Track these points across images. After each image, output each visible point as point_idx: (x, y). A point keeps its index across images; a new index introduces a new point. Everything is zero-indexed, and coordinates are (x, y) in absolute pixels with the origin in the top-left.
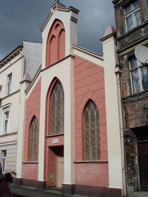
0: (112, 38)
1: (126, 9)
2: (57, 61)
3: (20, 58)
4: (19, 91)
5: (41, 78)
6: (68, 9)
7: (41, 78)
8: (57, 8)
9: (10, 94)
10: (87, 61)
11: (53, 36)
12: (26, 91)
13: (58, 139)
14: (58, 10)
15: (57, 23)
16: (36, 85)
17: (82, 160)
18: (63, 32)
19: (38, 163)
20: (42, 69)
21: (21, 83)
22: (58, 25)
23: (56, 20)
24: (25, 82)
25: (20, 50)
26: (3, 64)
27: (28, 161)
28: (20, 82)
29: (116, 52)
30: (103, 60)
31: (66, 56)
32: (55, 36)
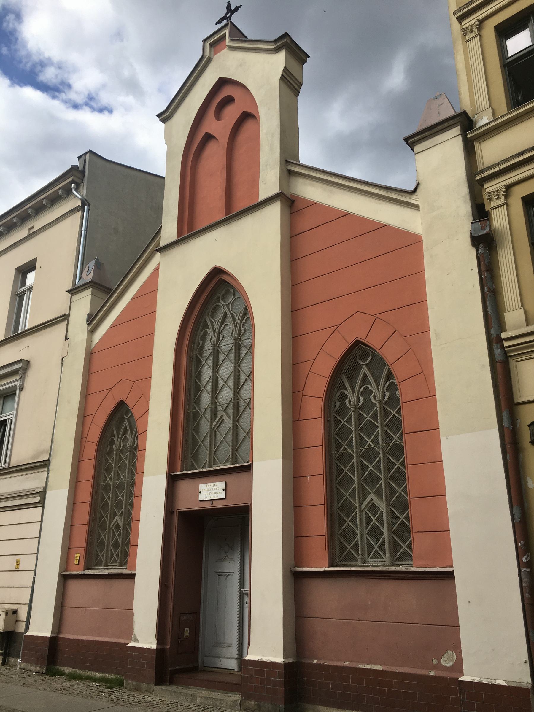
0: (456, 131)
1: (482, 144)
2: (222, 217)
3: (72, 211)
4: (65, 317)
5: (157, 270)
6: (275, 41)
7: (157, 270)
8: (227, 41)
9: (20, 331)
10: (347, 214)
11: (209, 137)
12: (90, 319)
13: (222, 485)
14: (231, 48)
15: (227, 91)
16: (133, 299)
17: (326, 563)
18: (249, 125)
19: (133, 576)
20: (162, 244)
21: (74, 291)
22: (229, 100)
23: (222, 83)
24: (89, 291)
25: (72, 182)
26: (29, 211)
27: (86, 568)
28: (67, 289)
29: (503, 66)
30: (416, 207)
31: (263, 196)
32: (214, 134)
